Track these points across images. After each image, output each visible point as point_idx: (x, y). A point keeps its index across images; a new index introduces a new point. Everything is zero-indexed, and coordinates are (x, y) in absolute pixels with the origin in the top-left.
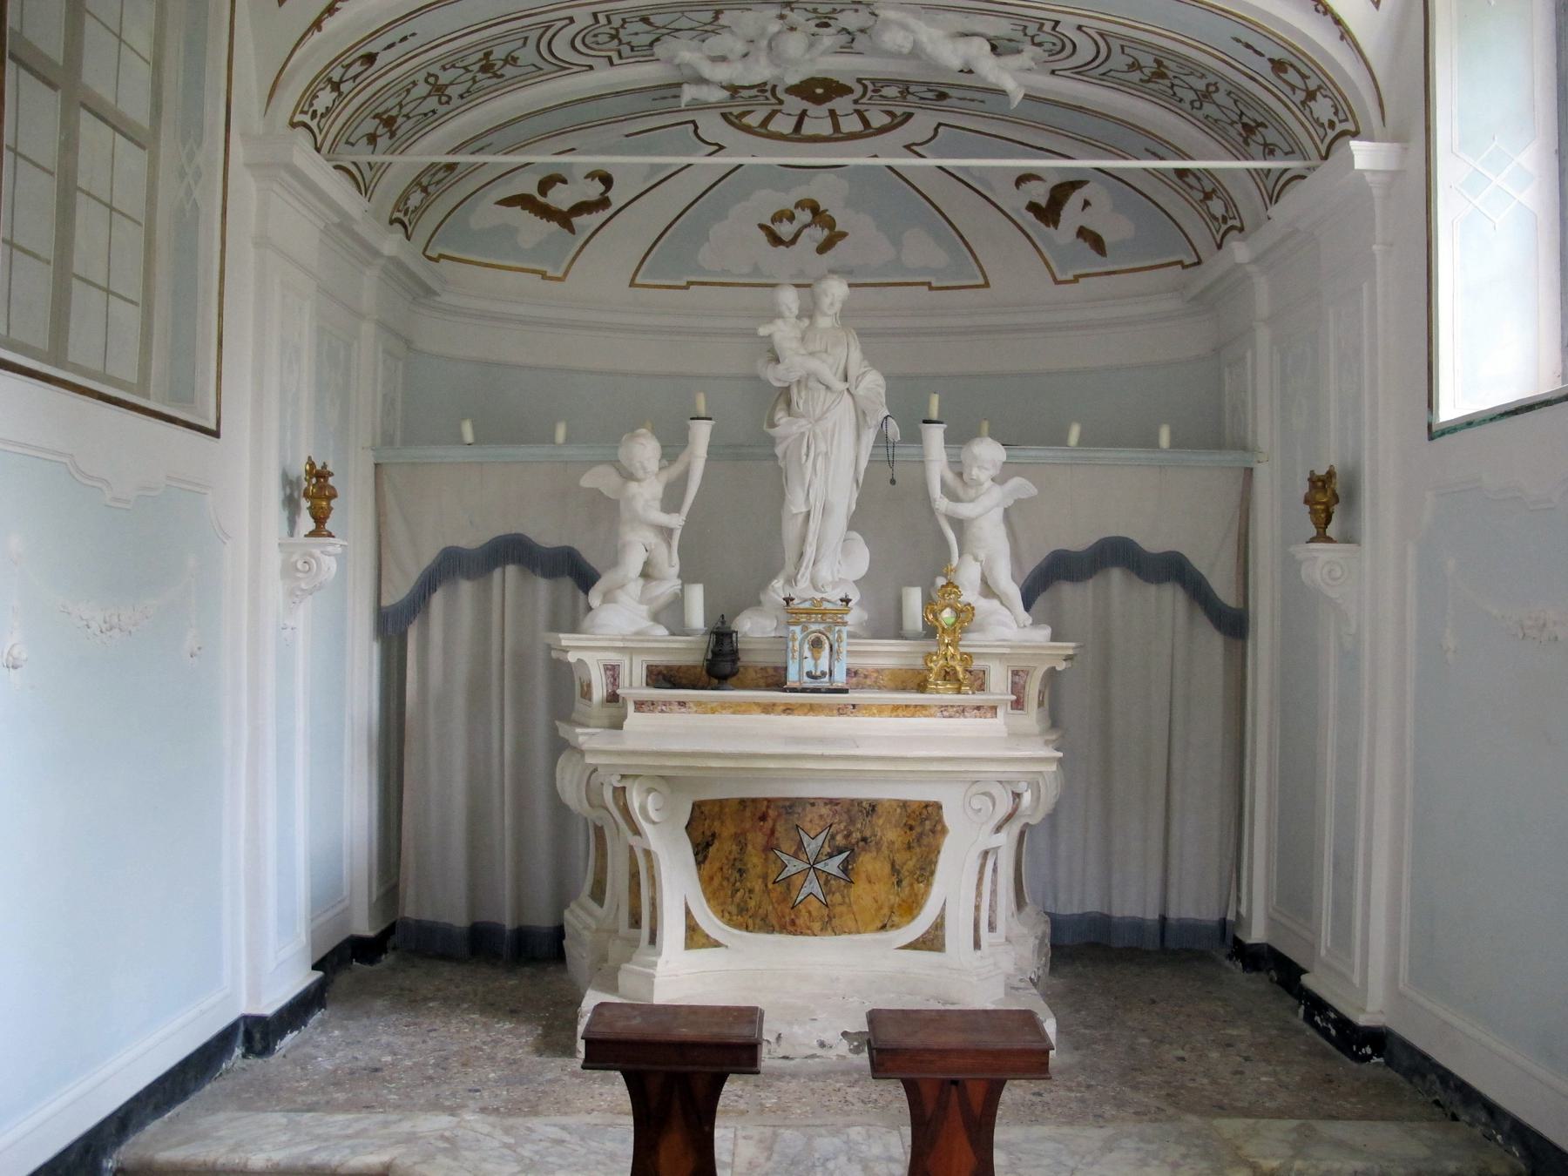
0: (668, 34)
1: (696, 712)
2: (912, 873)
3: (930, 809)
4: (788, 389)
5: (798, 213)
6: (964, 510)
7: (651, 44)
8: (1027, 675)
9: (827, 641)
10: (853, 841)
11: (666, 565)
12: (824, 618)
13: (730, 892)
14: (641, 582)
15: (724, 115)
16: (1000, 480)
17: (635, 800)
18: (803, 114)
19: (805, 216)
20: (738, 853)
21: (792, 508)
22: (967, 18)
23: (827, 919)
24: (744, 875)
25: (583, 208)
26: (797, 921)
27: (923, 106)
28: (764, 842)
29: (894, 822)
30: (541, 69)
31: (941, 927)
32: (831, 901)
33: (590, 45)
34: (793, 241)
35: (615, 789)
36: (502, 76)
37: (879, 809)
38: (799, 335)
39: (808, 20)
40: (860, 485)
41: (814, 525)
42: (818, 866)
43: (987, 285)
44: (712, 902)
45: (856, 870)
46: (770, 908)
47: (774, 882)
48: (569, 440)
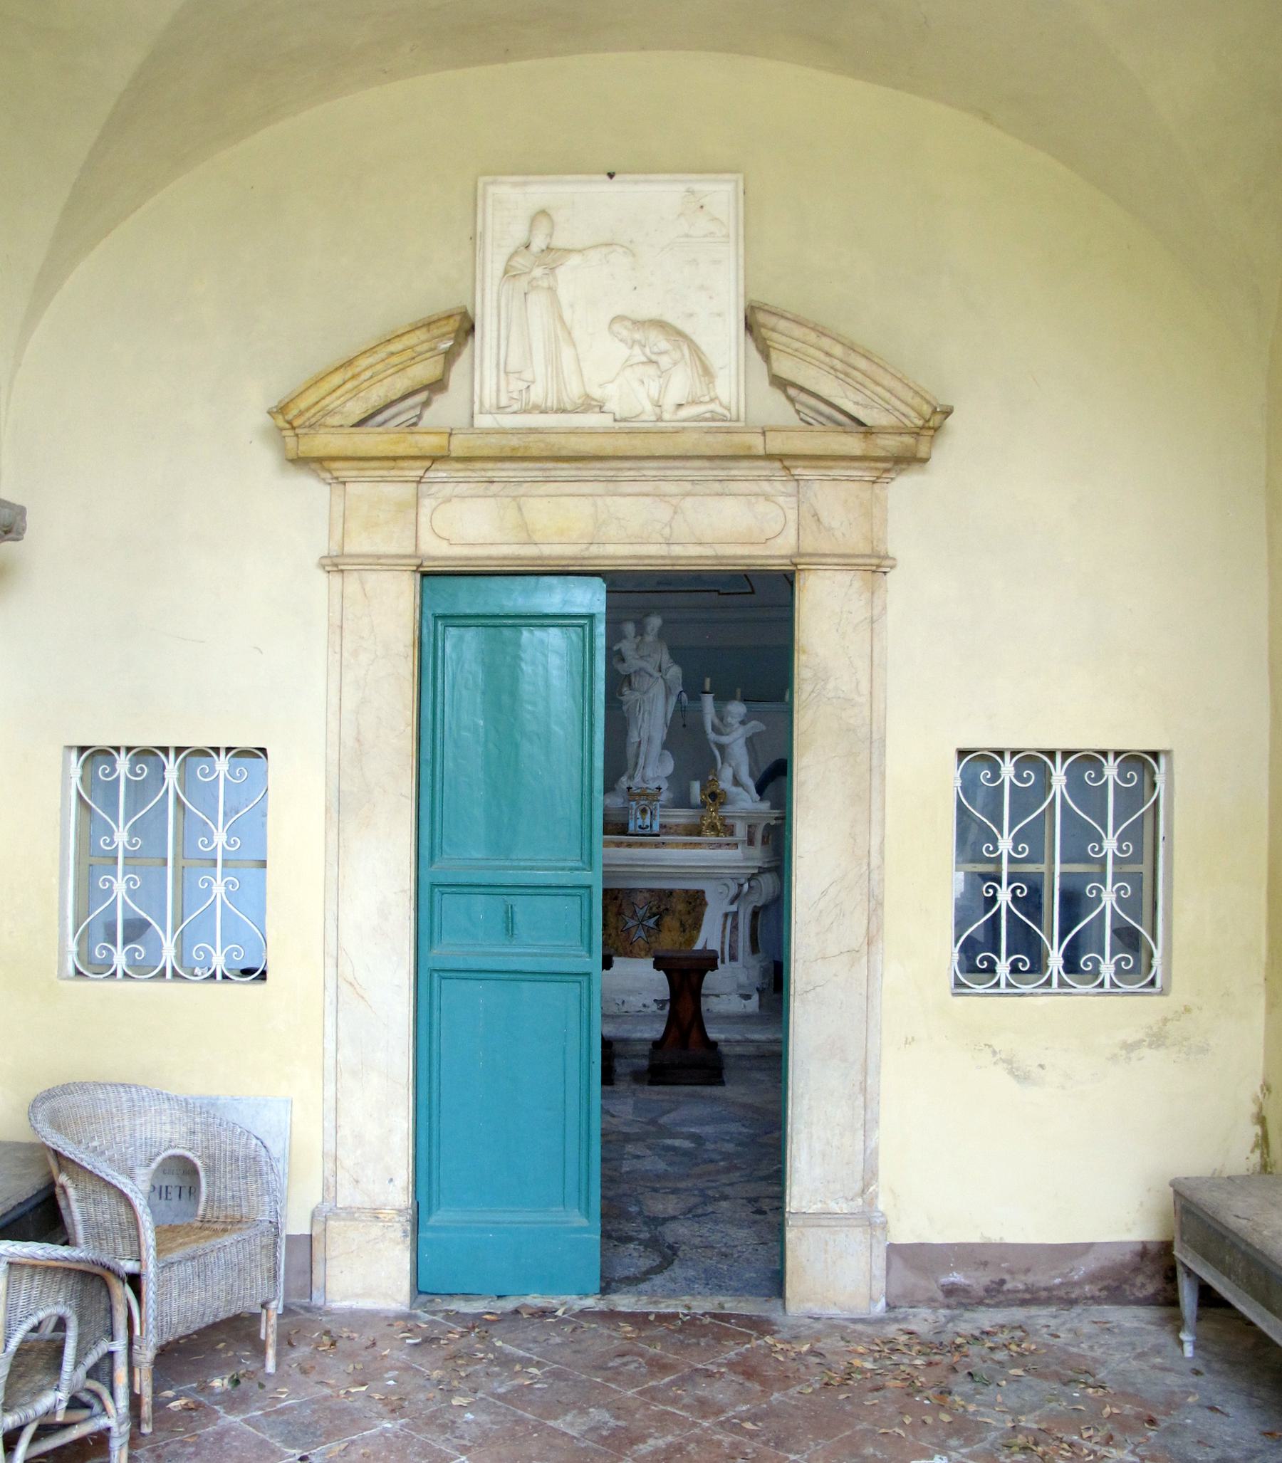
6: (724, 740)
16: (743, 723)
37: (674, 894)
41: (643, 748)
42: (644, 923)
46: (620, 944)
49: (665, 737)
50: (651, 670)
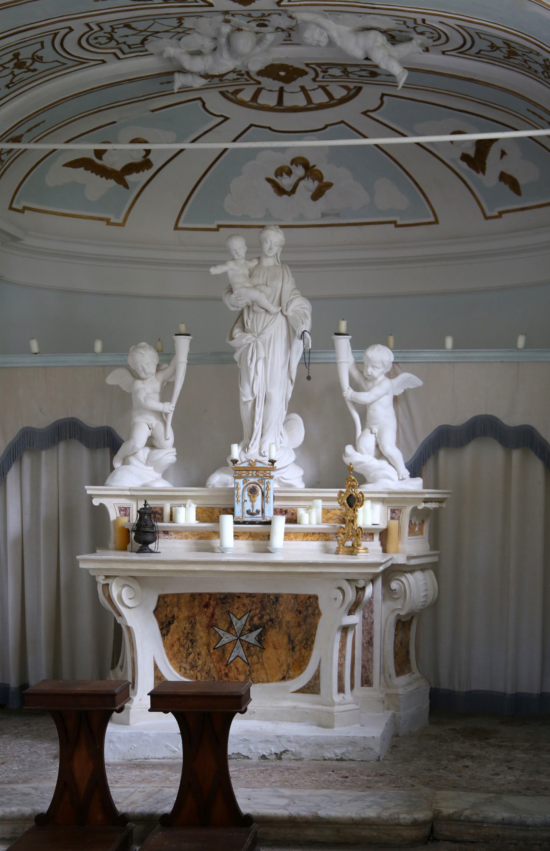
0: (151, 35)
1: (175, 538)
2: (301, 642)
3: (311, 599)
4: (241, 314)
5: (293, 168)
6: (364, 397)
7: (143, 42)
8: (400, 512)
9: (260, 490)
10: (265, 621)
11: (163, 439)
12: (258, 474)
13: (185, 655)
14: (147, 450)
15: (222, 93)
16: (391, 375)
17: (114, 592)
18: (281, 91)
19: (299, 171)
20: (190, 629)
21: (243, 398)
22: (360, 16)
23: (248, 673)
24: (195, 644)
25: (131, 168)
26: (230, 675)
27: (364, 81)
28: (207, 622)
29: (290, 608)
30: (64, 64)
31: (318, 678)
32: (251, 661)
33: (95, 45)
34: (293, 191)
35: (104, 585)
36: (35, 70)
37: (280, 599)
38: (247, 272)
39: (249, 22)
40: (294, 381)
41: (259, 410)
42: (243, 638)
43: (436, 222)
44: (173, 661)
45: (266, 640)
46: (212, 665)
47: (214, 649)
48: (105, 350)
49: (290, 396)
50: (266, 303)
